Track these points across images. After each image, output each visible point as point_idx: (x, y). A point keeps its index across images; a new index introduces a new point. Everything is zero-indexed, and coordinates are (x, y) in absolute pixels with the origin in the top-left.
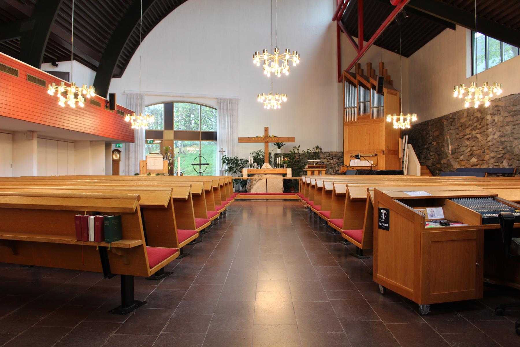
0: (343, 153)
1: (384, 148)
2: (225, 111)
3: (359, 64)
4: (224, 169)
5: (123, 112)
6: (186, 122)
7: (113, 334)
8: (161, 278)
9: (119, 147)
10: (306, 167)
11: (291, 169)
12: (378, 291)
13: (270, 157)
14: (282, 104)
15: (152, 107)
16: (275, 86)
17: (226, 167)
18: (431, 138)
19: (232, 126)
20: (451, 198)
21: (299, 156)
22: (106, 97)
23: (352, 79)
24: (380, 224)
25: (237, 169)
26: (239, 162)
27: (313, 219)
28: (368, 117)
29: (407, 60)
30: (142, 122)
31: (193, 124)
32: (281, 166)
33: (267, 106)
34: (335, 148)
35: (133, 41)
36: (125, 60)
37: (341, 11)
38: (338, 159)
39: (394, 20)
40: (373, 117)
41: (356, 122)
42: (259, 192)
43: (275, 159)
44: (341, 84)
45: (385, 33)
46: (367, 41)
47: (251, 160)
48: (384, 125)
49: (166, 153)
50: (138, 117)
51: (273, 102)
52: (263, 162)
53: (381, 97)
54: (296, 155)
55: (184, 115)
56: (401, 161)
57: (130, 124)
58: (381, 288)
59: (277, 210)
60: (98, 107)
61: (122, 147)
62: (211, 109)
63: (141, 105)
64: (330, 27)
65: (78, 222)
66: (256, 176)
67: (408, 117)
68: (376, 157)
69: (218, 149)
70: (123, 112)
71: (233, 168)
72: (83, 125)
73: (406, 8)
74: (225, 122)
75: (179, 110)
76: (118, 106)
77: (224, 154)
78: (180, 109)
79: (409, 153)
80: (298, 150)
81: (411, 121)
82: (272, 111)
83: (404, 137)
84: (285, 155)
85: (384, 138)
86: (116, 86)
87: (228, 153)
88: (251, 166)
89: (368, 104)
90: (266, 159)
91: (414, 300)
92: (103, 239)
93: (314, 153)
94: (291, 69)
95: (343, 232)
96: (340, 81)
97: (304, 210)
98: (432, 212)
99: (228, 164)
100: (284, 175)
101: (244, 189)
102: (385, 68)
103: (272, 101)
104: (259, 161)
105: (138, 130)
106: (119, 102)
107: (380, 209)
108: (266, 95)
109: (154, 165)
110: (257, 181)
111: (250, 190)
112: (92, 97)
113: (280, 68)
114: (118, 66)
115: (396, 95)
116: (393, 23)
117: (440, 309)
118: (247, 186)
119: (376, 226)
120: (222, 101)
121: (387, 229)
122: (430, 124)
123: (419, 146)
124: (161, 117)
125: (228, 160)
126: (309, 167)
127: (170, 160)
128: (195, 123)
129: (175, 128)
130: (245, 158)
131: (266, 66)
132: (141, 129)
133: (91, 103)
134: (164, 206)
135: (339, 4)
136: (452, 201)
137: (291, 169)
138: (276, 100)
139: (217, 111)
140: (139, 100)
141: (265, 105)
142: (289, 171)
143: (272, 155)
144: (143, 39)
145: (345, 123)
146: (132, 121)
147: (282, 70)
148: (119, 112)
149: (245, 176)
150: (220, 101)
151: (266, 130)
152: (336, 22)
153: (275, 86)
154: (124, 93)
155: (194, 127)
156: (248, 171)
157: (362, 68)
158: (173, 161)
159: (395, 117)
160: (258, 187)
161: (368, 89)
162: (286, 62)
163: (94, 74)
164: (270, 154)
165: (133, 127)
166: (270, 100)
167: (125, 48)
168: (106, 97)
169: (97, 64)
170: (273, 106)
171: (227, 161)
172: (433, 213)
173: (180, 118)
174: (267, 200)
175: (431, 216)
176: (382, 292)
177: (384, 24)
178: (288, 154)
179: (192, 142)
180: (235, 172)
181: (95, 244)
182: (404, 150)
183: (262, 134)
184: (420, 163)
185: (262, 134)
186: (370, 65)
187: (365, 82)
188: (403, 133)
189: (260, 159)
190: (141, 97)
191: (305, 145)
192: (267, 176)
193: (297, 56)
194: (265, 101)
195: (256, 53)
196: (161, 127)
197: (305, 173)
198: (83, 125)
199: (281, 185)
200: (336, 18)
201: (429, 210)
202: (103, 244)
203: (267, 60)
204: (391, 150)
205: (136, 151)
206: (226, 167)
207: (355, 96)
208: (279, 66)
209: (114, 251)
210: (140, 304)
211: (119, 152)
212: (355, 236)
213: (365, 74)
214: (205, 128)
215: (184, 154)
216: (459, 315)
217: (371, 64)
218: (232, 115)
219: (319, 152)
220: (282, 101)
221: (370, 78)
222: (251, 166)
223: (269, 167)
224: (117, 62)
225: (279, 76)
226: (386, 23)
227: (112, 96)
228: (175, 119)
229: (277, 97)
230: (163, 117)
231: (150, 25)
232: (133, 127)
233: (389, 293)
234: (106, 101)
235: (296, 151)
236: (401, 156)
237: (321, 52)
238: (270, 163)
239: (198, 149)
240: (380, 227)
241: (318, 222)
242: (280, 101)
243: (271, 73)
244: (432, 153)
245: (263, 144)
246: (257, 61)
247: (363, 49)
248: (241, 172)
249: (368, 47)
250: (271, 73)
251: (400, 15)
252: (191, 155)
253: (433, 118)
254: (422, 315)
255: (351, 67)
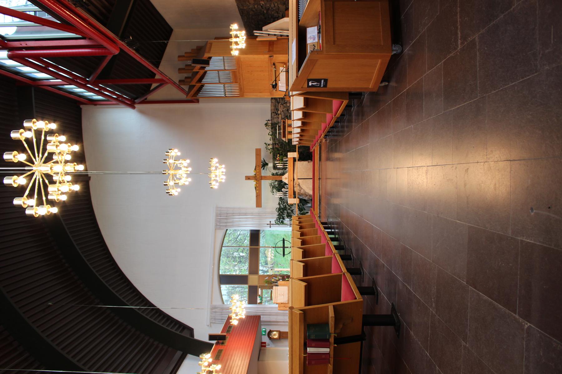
0: (272, 98)
1: (267, 56)
2: (229, 221)
3: (180, 81)
4: (289, 223)
5: (228, 327)
6: (241, 261)
7: (412, 333)
8: (377, 289)
9: (265, 331)
10: (284, 139)
11: (289, 153)
12: (386, 86)
13: (277, 174)
14: (221, 163)
15: (225, 298)
16: (201, 172)
17: (287, 220)
18: (256, 6)
19: (243, 213)
20: (298, 20)
21: (275, 144)
22: (213, 345)
23: (195, 89)
24: (322, 86)
25: (289, 209)
26: (282, 206)
27: (335, 133)
28: (234, 73)
29: (177, 31)
30: (239, 307)
31: (244, 254)
32: (285, 164)
33: (222, 179)
34: (268, 107)
35: (156, 316)
36: (175, 325)
37: (124, 100)
38: (279, 103)
39: (134, 49)
40: (234, 68)
41: (240, 85)
42: (311, 186)
43: (279, 169)
44: (200, 100)
45: (147, 59)
46: (155, 75)
47: (279, 195)
48: (242, 56)
49: (271, 283)
50: (233, 311)
51: (218, 173)
52: (281, 181)
53: (214, 59)
54: (275, 147)
55: (234, 263)
56: (280, 38)
57: (241, 320)
58: (383, 84)
59: (330, 168)
60: (223, 352)
61: (265, 328)
62: (227, 235)
63: (222, 309)
64: (142, 112)
65: (313, 362)
66: (296, 189)
67: (233, 33)
68: (277, 64)
69: (268, 228)
70: (228, 327)
71: (288, 213)
72: (241, 368)
73: (122, 38)
74: (240, 221)
75: (227, 269)
76: (222, 332)
77: (273, 222)
78: (227, 267)
79: (272, 29)
80: (269, 145)
81: (236, 30)
82: (227, 174)
83: (256, 34)
84: (274, 158)
85: (256, 56)
86: (201, 334)
87: (272, 218)
88: (285, 194)
89: (221, 73)
90: (278, 178)
91: (388, 59)
92: (328, 340)
93: (272, 128)
94: (183, 157)
95: (335, 116)
96: (198, 101)
97: (328, 141)
98: (311, 38)
99: (284, 219)
100: (294, 160)
101: (310, 202)
102: (184, 54)
103: (217, 174)
104: (280, 186)
105: (247, 312)
106: (218, 330)
107: (308, 86)
108: (211, 180)
109: (283, 295)
110: (302, 188)
111: (310, 196)
112: (211, 357)
113: (183, 169)
114: (181, 331)
115: (211, 44)
116: (137, 50)
117: (397, 35)
118: (306, 199)
119: (325, 90)
120: (218, 224)
121: (326, 81)
122: (242, 8)
123: (266, 18)
124: (236, 288)
125: (280, 218)
126: (284, 136)
127: (279, 279)
128: (242, 252)
129: (246, 273)
130: (278, 201)
131: (181, 182)
132: (246, 308)
133: (217, 359)
134: (305, 286)
135: (118, 103)
136: (301, 19)
137: (289, 153)
138: (216, 169)
139: (229, 229)
140: (216, 310)
141: (221, 180)
142: (291, 155)
143: (275, 172)
144: (154, 306)
145: (242, 94)
146: (238, 318)
147: (184, 167)
148: (228, 331)
149: (295, 201)
150: (218, 227)
151: (248, 178)
152: (136, 106)
153: (201, 172)
154: (210, 326)
155: (245, 254)
156: (291, 198)
157: (183, 79)
158: (280, 276)
159: (234, 46)
160: (307, 188)
161: (205, 72)
162: (177, 162)
163: (189, 356)
164: (273, 174)
165: (244, 317)
166: (216, 176)
167: (163, 324)
168: (213, 345)
169: (179, 353)
170: (222, 172)
171: (280, 220)
172: (312, 37)
173: (236, 268)
174: (319, 179)
175: (314, 39)
176: (387, 83)
177: (138, 59)
178: (274, 155)
179: (261, 255)
180: (292, 211)
181: (332, 348)
182: (269, 34)
183: (253, 183)
184: (283, 17)
185: (253, 183)
186: (180, 70)
187: (198, 76)
188: (250, 36)
189: (279, 184)
190: (213, 308)
191: (262, 138)
192: (295, 178)
193: (170, 151)
194: (217, 181)
195: (167, 193)
196: (245, 288)
197: (290, 140)
198: (241, 368)
199: (305, 163)
200: (132, 106)
201: (309, 41)
202: (332, 340)
203: (175, 181)
204: (269, 49)
205: (270, 314)
206: (287, 220)
207: (214, 85)
208: (181, 172)
209: (338, 331)
210: (393, 308)
211: (270, 332)
212: (337, 106)
213: (190, 75)
214: (247, 242)
215: (275, 264)
216: (402, 17)
217: (180, 69)
218: (233, 214)
219: (271, 124)
220: (217, 163)
221: (194, 71)
222: (285, 194)
223: (286, 175)
224: (178, 333)
225: (190, 169)
226: (138, 57)
227: (212, 337)
228: (238, 273)
229: (213, 168)
230: (236, 286)
231: (139, 298)
232: (244, 317)
233: (387, 77)
234: (217, 344)
235: (271, 147)
236: (274, 38)
237: (167, 121)
238: (283, 174)
239: (270, 249)
240: (325, 86)
241: (337, 129)
242: (218, 165)
243: (187, 177)
244: (272, 5)
245: (263, 182)
246: (175, 192)
247: (164, 79)
248: (292, 205)
249: (161, 73)
250: (187, 177)
251: (130, 44)
252: (275, 256)
253: (235, 4)
254: (402, 51)
255: (182, 90)
